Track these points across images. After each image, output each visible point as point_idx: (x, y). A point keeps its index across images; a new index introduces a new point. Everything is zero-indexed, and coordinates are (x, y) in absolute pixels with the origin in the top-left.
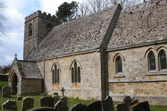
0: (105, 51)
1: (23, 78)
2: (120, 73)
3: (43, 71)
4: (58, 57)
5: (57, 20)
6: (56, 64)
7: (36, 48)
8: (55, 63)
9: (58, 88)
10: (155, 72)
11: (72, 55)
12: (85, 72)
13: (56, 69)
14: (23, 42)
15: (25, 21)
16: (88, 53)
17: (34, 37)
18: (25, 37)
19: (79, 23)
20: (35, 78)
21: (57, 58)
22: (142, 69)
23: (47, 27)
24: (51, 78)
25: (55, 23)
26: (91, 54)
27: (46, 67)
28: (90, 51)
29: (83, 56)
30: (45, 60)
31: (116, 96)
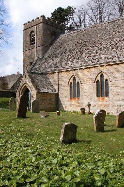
1: (38, 93)
3: (58, 84)
4: (77, 68)
5: (61, 28)
6: (75, 76)
7: (41, 59)
8: (74, 75)
9: (78, 103)
11: (98, 66)
12: (114, 85)
13: (76, 82)
14: (23, 53)
15: (24, 28)
16: (119, 64)
17: (38, 46)
18: (25, 47)
19: (95, 30)
20: (49, 92)
21: (77, 69)
23: (52, 35)
24: (69, 92)
25: (59, 31)
27: (60, 80)
28: (122, 62)
29: (112, 67)
30: (59, 72)
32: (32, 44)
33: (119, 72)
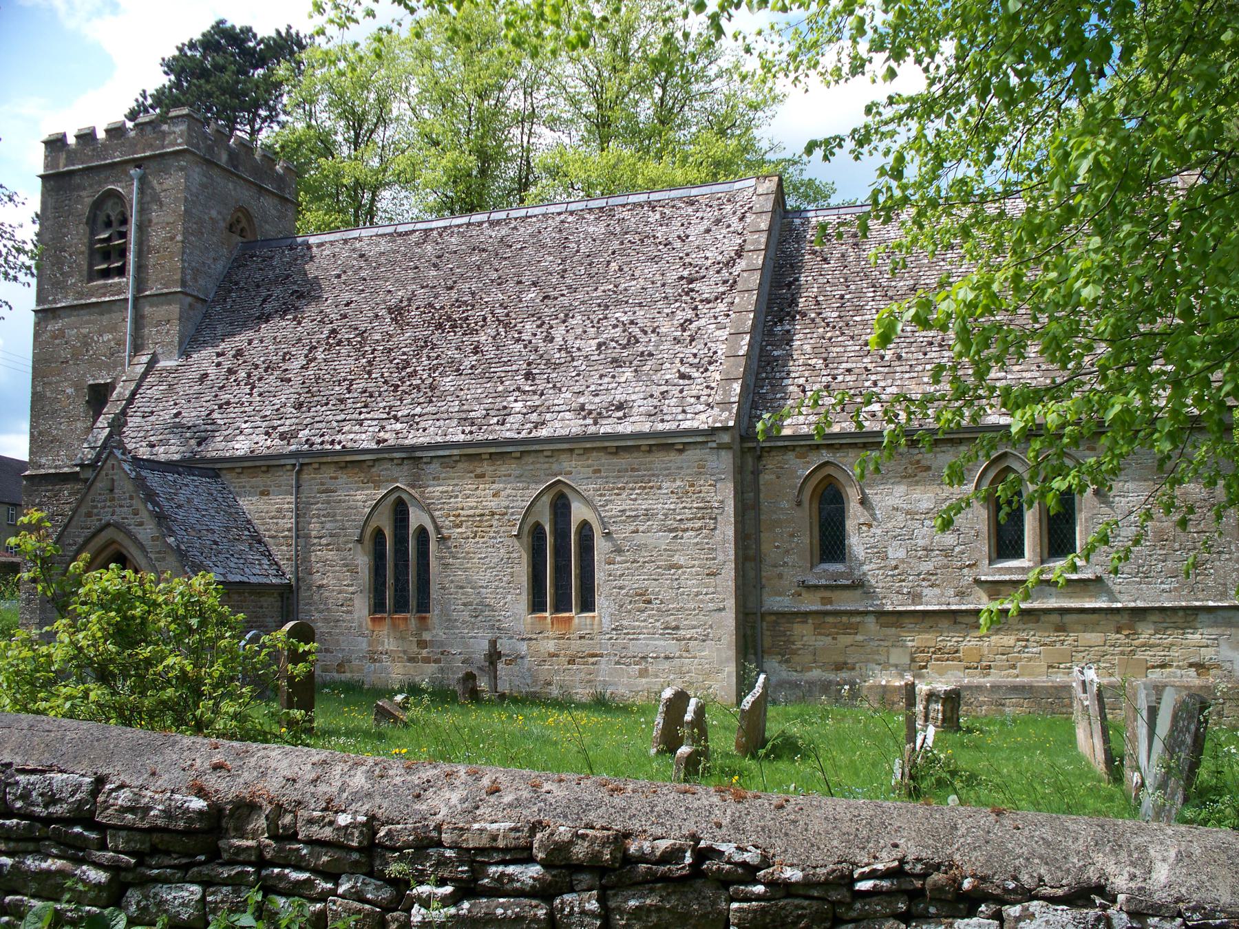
0: (751, 445)
2: (839, 567)
10: (1023, 568)
20: (253, 580)
22: (957, 549)
23: (231, 228)
26: (673, 456)
31: (806, 682)
32: (106, 274)
33: (651, 488)
